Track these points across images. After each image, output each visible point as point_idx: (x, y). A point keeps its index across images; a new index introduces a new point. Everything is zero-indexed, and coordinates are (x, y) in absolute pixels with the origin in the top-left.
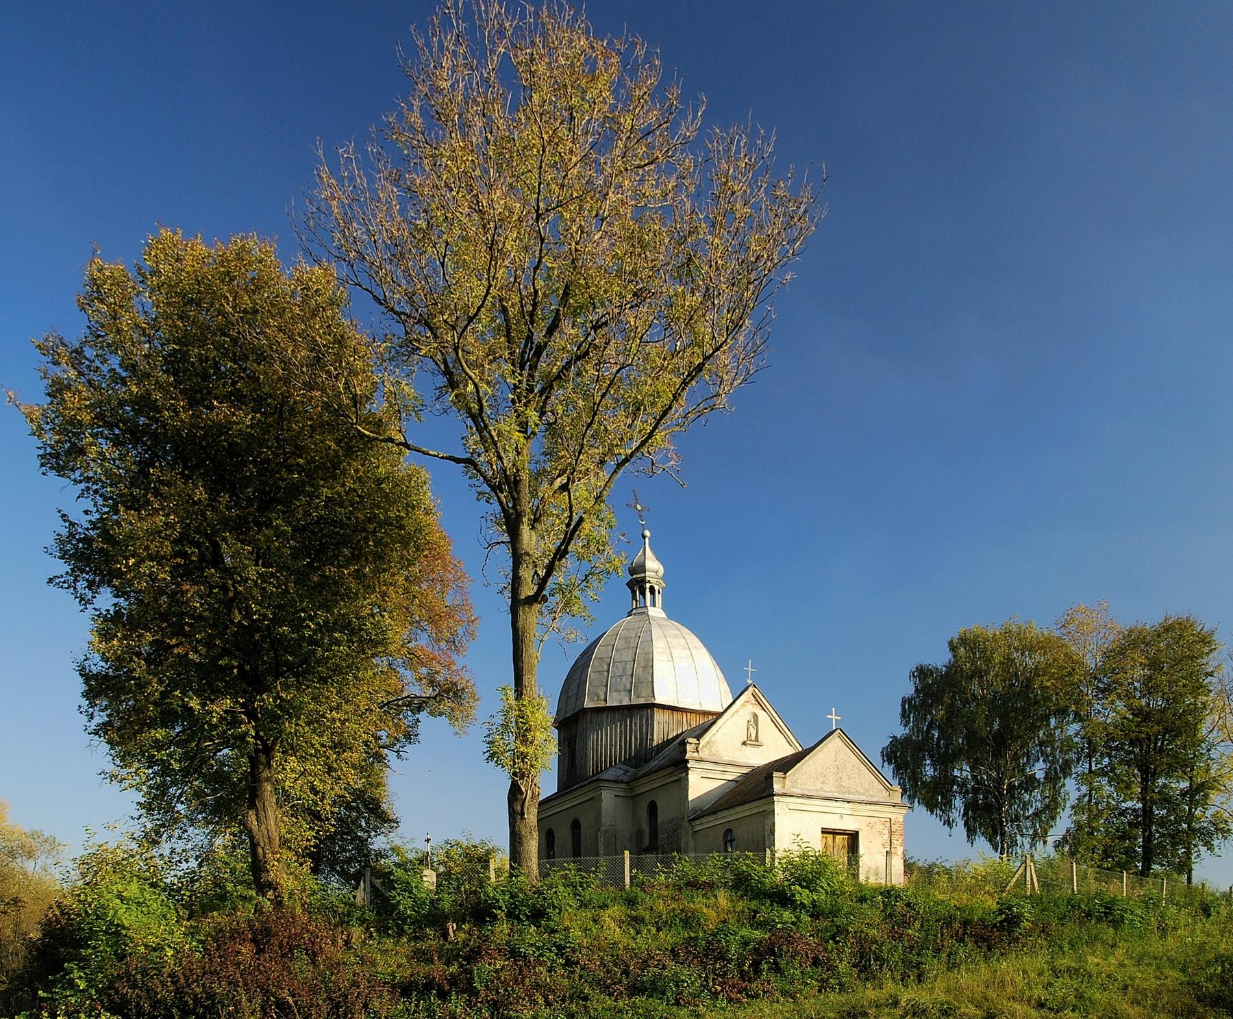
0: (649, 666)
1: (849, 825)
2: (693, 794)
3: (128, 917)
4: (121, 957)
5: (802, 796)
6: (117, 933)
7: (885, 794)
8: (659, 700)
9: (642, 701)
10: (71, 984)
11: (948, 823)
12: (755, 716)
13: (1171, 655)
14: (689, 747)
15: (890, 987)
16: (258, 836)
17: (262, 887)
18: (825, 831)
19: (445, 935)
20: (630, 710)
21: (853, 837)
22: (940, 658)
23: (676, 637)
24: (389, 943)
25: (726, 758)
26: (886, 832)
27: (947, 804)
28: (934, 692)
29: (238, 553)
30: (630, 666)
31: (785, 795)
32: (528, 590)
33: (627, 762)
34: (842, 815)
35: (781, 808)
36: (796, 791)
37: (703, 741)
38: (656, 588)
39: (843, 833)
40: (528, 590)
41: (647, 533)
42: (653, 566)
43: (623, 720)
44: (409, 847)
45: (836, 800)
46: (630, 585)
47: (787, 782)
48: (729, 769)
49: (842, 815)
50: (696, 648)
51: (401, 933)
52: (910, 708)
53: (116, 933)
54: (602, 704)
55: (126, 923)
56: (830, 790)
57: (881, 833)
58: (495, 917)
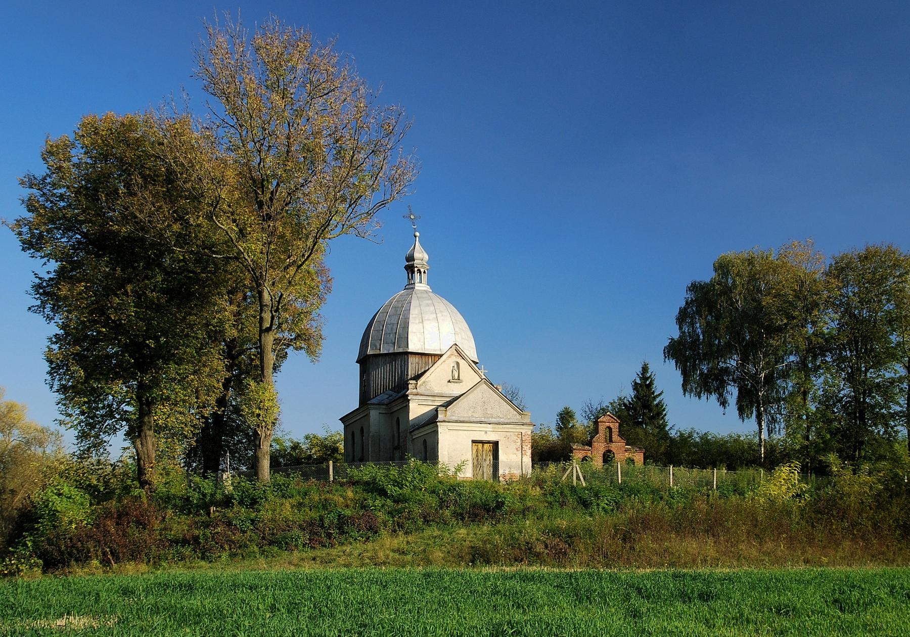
0: (406, 327)
1: (492, 437)
2: (412, 416)
3: (59, 504)
4: (55, 527)
5: (456, 422)
6: (54, 514)
7: (519, 417)
8: (412, 348)
9: (401, 350)
10: (25, 545)
11: (724, 403)
12: (458, 364)
13: (868, 273)
14: (410, 386)
15: (339, 548)
16: (141, 453)
17: (143, 484)
18: (474, 442)
19: (208, 514)
20: (395, 355)
21: (496, 444)
22: (707, 275)
23: (428, 305)
24: (183, 517)
25: (437, 391)
26: (519, 440)
27: (720, 391)
28: (704, 301)
29: (147, 280)
30: (395, 327)
31: (444, 421)
32: (267, 325)
33: (393, 389)
34: (486, 432)
35: (442, 429)
36: (454, 418)
37: (420, 382)
38: (422, 270)
39: (489, 442)
40: (267, 325)
41: (417, 234)
42: (421, 256)
43: (391, 363)
44: (287, 437)
45: (481, 422)
46: (407, 268)
47: (448, 413)
48: (437, 399)
49: (486, 432)
50: (441, 312)
51: (189, 513)
52: (683, 317)
53: (54, 515)
54: (377, 352)
55: (59, 509)
56: (478, 416)
57: (515, 442)
58: (233, 503)
